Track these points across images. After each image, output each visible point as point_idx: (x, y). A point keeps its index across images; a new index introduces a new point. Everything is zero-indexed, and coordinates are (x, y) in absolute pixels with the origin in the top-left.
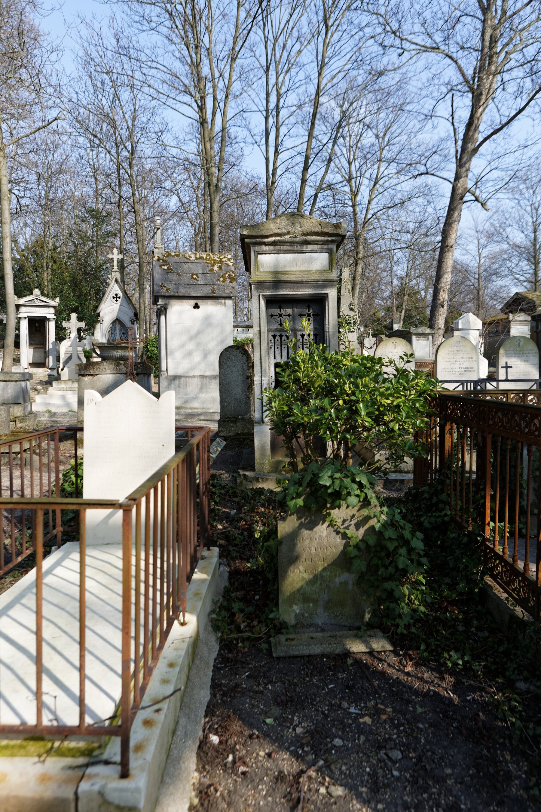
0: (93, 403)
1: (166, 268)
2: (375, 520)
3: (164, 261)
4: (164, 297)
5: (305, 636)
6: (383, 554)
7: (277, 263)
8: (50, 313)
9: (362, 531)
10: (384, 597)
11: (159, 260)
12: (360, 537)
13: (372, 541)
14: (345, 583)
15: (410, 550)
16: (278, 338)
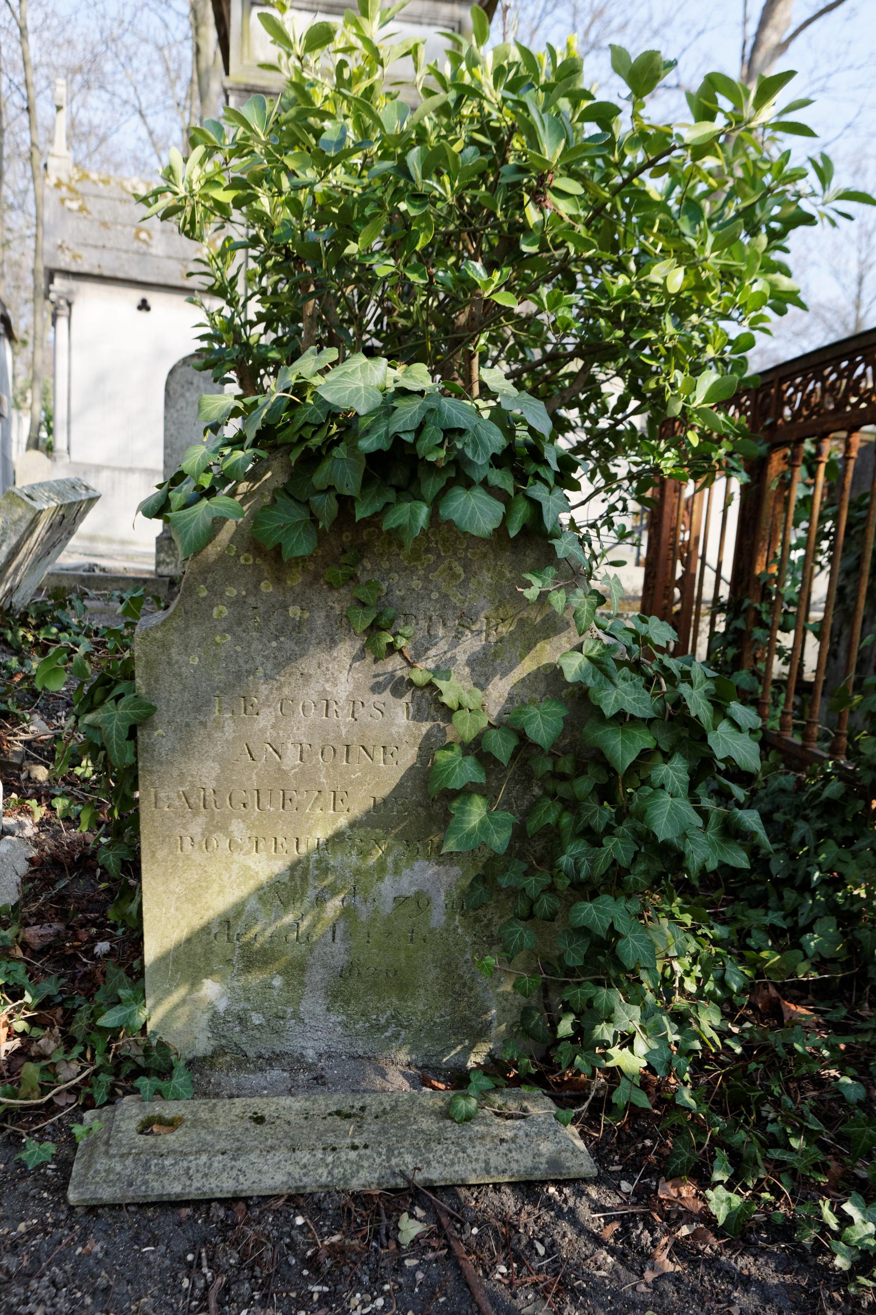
2: (565, 640)
3: (71, 189)
4: (67, 274)
5: (229, 1113)
6: (583, 786)
9: (500, 689)
10: (574, 960)
11: (58, 185)
12: (494, 711)
13: (544, 725)
14: (420, 902)
15: (703, 767)
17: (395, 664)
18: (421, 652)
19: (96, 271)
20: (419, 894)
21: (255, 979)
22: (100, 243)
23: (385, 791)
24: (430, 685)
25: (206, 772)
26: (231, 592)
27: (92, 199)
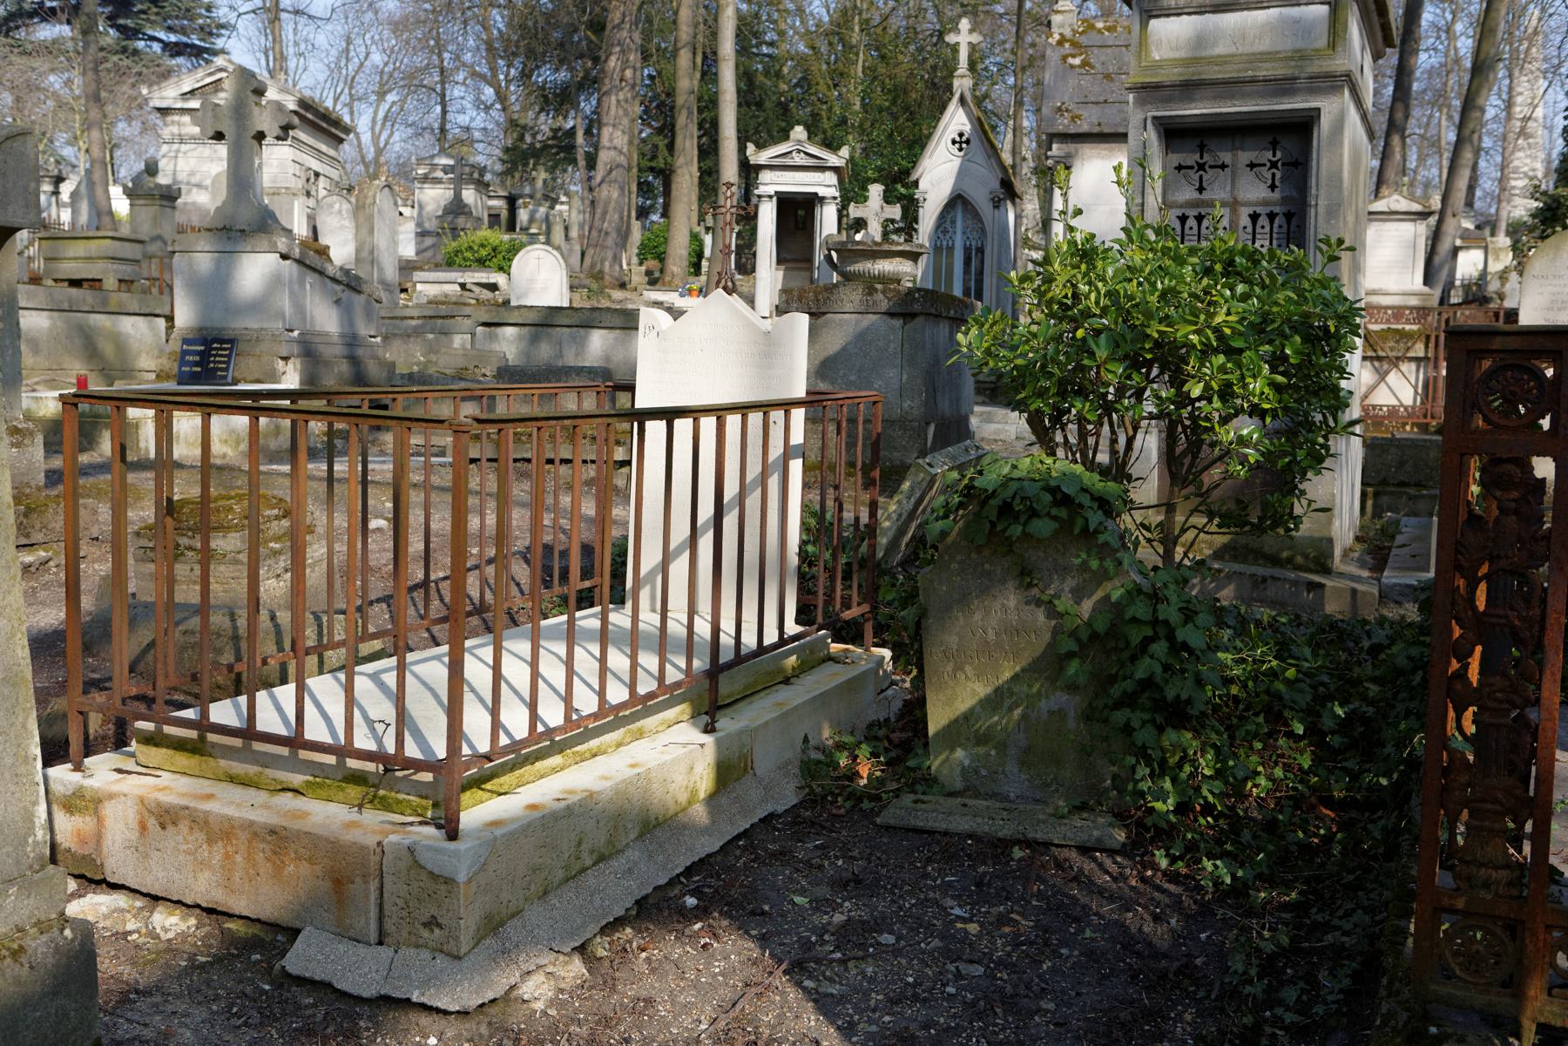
0: (654, 333)
1: (1077, 61)
3: (1074, 44)
4: (1065, 137)
7: (1200, 40)
8: (825, 185)
9: (1087, 606)
11: (1060, 43)
14: (1059, 714)
16: (1191, 222)
17: (1035, 591)
18: (1047, 586)
19: (1096, 130)
20: (1060, 710)
21: (981, 750)
22: (1101, 99)
23: (1037, 654)
24: (1050, 602)
25: (953, 640)
26: (959, 558)
27: (1096, 51)
